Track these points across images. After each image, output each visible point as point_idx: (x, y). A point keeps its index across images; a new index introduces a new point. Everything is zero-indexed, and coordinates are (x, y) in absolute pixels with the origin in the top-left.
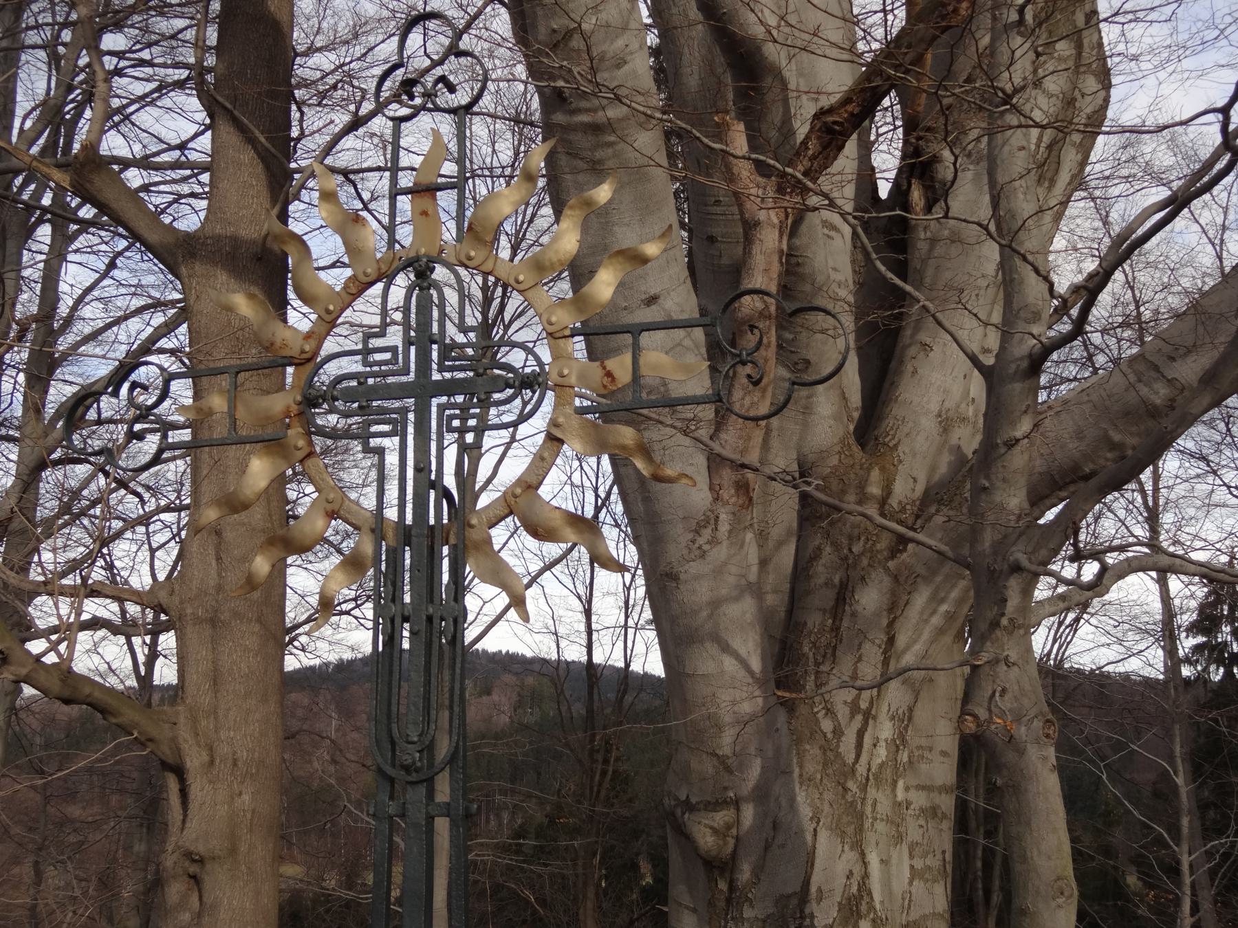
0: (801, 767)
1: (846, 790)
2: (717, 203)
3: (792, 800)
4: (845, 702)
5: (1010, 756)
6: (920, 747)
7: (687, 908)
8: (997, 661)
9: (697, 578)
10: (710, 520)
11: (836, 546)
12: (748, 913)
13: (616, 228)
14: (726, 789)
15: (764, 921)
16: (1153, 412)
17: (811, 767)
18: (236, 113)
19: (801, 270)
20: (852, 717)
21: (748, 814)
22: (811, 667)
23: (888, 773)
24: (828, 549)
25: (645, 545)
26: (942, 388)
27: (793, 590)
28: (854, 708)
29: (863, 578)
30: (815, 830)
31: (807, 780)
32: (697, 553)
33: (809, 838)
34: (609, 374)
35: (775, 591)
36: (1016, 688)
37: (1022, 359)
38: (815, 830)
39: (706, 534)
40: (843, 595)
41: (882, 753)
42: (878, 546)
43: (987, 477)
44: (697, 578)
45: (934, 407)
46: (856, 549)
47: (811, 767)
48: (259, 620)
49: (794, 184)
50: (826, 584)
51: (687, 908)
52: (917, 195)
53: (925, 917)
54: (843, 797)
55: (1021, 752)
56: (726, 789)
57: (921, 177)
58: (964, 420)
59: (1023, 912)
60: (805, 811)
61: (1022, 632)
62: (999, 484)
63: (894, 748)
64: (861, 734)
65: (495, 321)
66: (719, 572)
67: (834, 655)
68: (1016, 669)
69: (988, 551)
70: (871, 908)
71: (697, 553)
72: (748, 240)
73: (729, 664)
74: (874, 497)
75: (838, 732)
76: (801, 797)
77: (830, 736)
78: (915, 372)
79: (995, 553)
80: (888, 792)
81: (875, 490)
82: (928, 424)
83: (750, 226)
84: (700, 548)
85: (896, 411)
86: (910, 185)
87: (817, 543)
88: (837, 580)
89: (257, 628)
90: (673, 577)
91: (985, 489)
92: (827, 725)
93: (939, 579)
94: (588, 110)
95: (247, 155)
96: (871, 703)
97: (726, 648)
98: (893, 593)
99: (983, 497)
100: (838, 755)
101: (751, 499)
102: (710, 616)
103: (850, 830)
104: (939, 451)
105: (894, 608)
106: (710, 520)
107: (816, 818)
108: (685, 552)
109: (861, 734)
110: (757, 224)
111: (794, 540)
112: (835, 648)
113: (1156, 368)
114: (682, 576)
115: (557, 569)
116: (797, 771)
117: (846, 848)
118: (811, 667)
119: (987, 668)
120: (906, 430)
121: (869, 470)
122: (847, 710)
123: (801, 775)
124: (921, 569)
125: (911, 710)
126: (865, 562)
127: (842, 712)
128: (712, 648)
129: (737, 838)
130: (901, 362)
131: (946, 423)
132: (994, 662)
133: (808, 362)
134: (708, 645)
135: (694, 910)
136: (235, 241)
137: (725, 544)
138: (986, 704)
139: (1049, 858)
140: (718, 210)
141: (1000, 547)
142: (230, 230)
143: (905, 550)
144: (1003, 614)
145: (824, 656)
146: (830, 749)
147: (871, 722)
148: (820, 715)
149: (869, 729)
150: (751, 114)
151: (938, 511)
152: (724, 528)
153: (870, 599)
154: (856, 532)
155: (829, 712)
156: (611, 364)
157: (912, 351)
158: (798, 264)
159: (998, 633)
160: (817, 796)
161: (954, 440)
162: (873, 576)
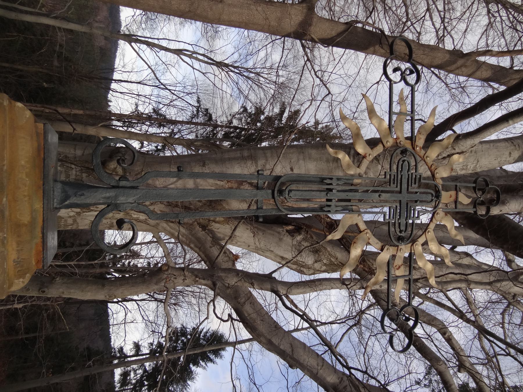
5: (155, 281)
7: (84, 152)
8: (185, 277)
12: (84, 175)
13: (315, 162)
14: (130, 173)
15: (81, 180)
16: (236, 298)
18: (347, 32)
24: (201, 204)
34: (399, 267)
41: (135, 216)
48: (190, 11)
51: (84, 152)
52: (290, 227)
53: (78, 224)
55: (156, 284)
56: (130, 173)
57: (295, 229)
59: (103, 286)
69: (219, 275)
70: (84, 212)
78: (247, 229)
79: (218, 277)
86: (293, 226)
89: (187, 10)
91: (238, 275)
93: (190, 236)
95: (334, 33)
99: (235, 274)
104: (223, 234)
113: (248, 299)
115: (153, 75)
119: (183, 273)
124: (194, 232)
129: (111, 174)
135: (83, 155)
136: (310, 25)
139: (122, 293)
141: (220, 278)
142: (314, 24)
156: (402, 268)
159: (194, 277)
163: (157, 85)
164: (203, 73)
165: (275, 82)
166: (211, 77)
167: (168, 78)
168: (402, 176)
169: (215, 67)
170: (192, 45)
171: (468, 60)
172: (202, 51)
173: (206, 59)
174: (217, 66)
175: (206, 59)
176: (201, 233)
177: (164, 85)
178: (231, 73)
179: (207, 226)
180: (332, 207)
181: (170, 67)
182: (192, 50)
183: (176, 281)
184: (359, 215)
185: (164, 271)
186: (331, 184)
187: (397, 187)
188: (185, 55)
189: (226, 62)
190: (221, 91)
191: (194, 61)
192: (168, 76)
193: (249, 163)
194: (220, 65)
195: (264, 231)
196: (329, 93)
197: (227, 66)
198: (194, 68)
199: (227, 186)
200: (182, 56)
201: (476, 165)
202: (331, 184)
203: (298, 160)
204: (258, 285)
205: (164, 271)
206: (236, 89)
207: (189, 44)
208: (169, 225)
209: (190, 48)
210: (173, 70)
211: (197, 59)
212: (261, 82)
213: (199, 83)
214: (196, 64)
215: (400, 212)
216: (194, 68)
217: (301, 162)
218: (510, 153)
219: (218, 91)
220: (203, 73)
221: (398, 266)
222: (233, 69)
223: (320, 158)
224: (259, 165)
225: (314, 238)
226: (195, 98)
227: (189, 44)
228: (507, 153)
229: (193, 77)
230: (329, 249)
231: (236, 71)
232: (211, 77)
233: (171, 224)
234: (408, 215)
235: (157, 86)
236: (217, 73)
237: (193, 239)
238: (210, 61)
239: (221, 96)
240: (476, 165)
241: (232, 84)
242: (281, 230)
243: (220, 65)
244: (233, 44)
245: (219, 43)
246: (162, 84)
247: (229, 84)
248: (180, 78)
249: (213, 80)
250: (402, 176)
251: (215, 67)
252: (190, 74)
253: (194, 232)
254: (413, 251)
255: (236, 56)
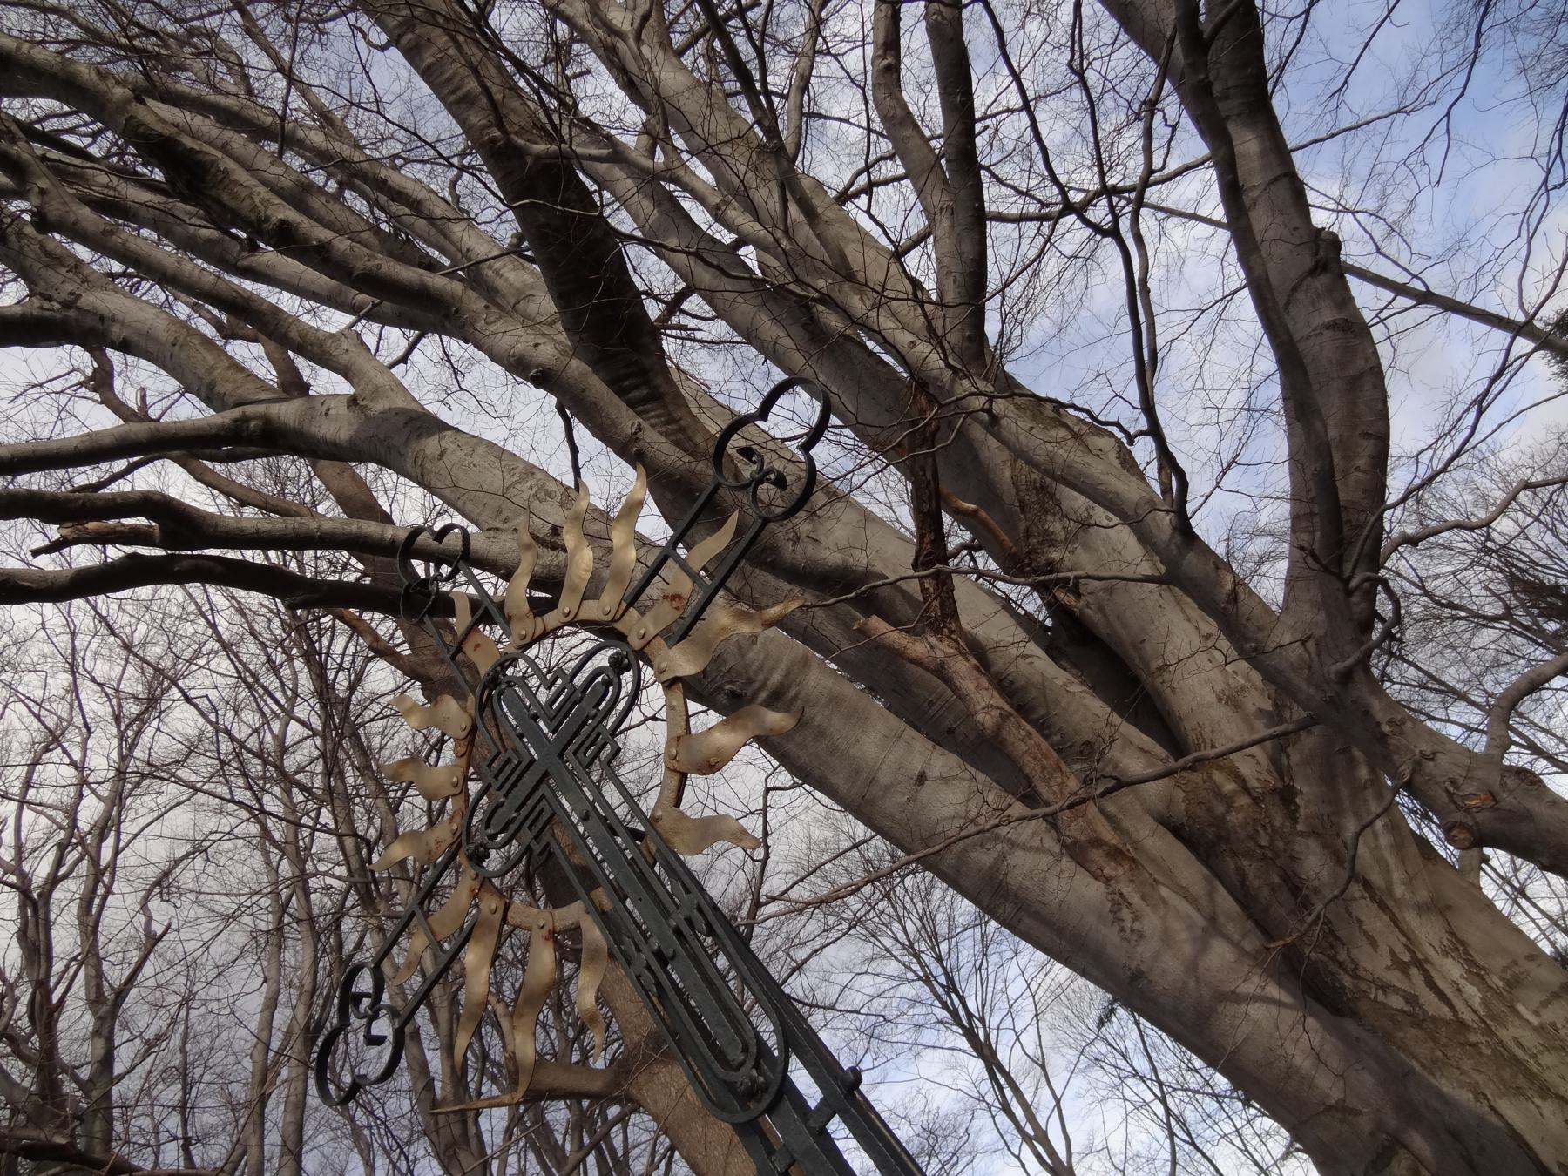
0: (1415, 1057)
1: (1474, 1046)
2: (931, 704)
3: (1440, 1095)
4: (1388, 968)
6: (1504, 970)
9: (1156, 957)
10: (1119, 902)
11: (1248, 854)
13: (852, 751)
17: (1424, 1051)
19: (1017, 685)
20: (1408, 976)
21: (1419, 1142)
22: (1332, 967)
23: (1498, 1006)
24: (1245, 863)
25: (1095, 972)
26: (1202, 676)
27: (1257, 923)
28: (1403, 967)
29: (1293, 858)
30: (1492, 1108)
31: (1434, 1066)
32: (1135, 937)
33: (1494, 1120)
35: (1244, 935)
36: (1459, 771)
37: (1172, 537)
38: (1492, 1108)
39: (1126, 914)
40: (1294, 886)
41: (1471, 990)
42: (1277, 824)
43: (1247, 640)
44: (1156, 957)
45: (1210, 697)
46: (1264, 842)
47: (1424, 1051)
49: (940, 613)
50: (1273, 890)
52: (1066, 598)
54: (1481, 1054)
55: (1528, 816)
58: (1242, 689)
60: (1464, 1096)
61: (1409, 724)
62: (1260, 635)
63: (1477, 979)
64: (1431, 984)
65: (970, 1022)
66: (1167, 937)
67: (1337, 938)
68: (1439, 756)
71: (1135, 937)
72: (948, 681)
73: (1256, 1011)
74: (1235, 792)
75: (1412, 999)
76: (1445, 1086)
77: (1408, 1009)
78: (1173, 690)
80: (1517, 1022)
81: (1229, 787)
82: (1219, 712)
83: (940, 671)
84: (1132, 931)
85: (1188, 726)
87: (1233, 866)
88: (1277, 880)
90: (1138, 976)
92: (1396, 1002)
93: (1347, 803)
94: (761, 689)
96: (1409, 950)
97: (1237, 998)
98: (1325, 846)
100: (1434, 1019)
101: (1133, 860)
102: (1198, 981)
103: (1521, 1081)
105: (1344, 858)
106: (1119, 902)
107: (1479, 1095)
108: (1125, 944)
109: (1431, 984)
110: (942, 665)
111: (1217, 882)
112: (1332, 932)
114: (1144, 968)
116: (1415, 1064)
117: (1538, 1101)
118: (1332, 967)
119: (1418, 778)
120: (1208, 730)
121: (1210, 777)
122: (1397, 973)
123: (1423, 1066)
124: (1326, 809)
125: (1452, 933)
126: (1281, 845)
127: (1395, 978)
128: (1229, 1009)
130: (1159, 694)
131: (1232, 700)
132: (1417, 767)
133: (1088, 743)
134: (1220, 1008)
137: (1148, 909)
138: (1452, 807)
140: (935, 708)
143: (1298, 806)
144: (1378, 724)
145: (1332, 947)
146: (1420, 1020)
147: (1428, 967)
148: (1381, 997)
149: (1433, 973)
150: (871, 603)
151: (1288, 757)
152: (1135, 899)
153: (1314, 864)
154: (1250, 829)
155: (1385, 988)
157: (1158, 681)
158: (1012, 682)
159: (1392, 741)
160: (1457, 1072)
161: (1251, 709)
162: (1297, 848)
163: (1187, 1147)
164: (1043, 1067)
165: (887, 896)
166: (1029, 1039)
167: (1144, 1137)
168: (518, 810)
169: (1002, 1055)
170: (1018, 1157)
171: (423, 665)
172: (1002, 1118)
173: (1008, 1092)
174: (994, 1054)
175: (1008, 1092)
176: (1307, 789)
177: (1168, 1124)
178: (972, 1008)
179: (1274, 791)
180: (687, 913)
181: (1118, 1160)
182: (1025, 1147)
183: (1458, 773)
184: (657, 820)
185: (1469, 829)
186: (649, 967)
187: (543, 796)
188: (1052, 1153)
189: (963, 1043)
190: (1034, 986)
191: (1042, 1121)
192: (1140, 1142)
193: (1015, 879)
194: (985, 1052)
195: (1135, 647)
196: (768, 790)
197: (970, 1034)
198: (1058, 1101)
199: (1120, 871)
200: (1062, 1154)
201: (518, 482)
202: (649, 967)
203: (888, 788)
204: (1218, 583)
205: (1469, 829)
206: (993, 959)
207: (1023, 1166)
208: (1389, 883)
209: (1027, 1154)
210: (1116, 1145)
211: (1031, 1118)
212: (919, 924)
213: (1072, 1054)
214: (1043, 1104)
215: (577, 734)
216: (1058, 1101)
217: (884, 778)
218: (441, 456)
219: (1040, 993)
220: (1043, 1067)
221: (675, 604)
222: (961, 1012)
223: (832, 753)
224: (994, 855)
225: (1022, 526)
226: (1110, 1030)
227: (1023, 1166)
228: (447, 457)
229: (1078, 1083)
230: (1008, 473)
231: (957, 1002)
232: (1029, 1039)
233: (1376, 879)
234: (569, 705)
235: (1193, 1144)
236: (1007, 1038)
237: (1344, 792)
238: (1002, 1081)
239: (1042, 975)
240: (518, 482)
241: (991, 978)
242: (1090, 612)
243: (985, 1052)
244: (913, 1068)
245: (945, 1102)
246: (1172, 1135)
247: (1000, 986)
248: (1114, 1112)
249: (1032, 1030)
250: (518, 810)
251: (1000, 1056)
252: (1079, 1096)
253: (1326, 809)
254: (624, 605)
255: (928, 1036)
